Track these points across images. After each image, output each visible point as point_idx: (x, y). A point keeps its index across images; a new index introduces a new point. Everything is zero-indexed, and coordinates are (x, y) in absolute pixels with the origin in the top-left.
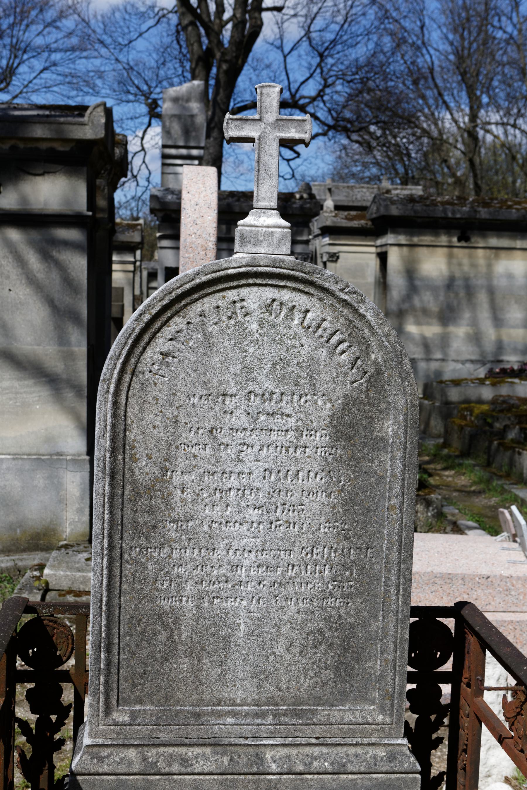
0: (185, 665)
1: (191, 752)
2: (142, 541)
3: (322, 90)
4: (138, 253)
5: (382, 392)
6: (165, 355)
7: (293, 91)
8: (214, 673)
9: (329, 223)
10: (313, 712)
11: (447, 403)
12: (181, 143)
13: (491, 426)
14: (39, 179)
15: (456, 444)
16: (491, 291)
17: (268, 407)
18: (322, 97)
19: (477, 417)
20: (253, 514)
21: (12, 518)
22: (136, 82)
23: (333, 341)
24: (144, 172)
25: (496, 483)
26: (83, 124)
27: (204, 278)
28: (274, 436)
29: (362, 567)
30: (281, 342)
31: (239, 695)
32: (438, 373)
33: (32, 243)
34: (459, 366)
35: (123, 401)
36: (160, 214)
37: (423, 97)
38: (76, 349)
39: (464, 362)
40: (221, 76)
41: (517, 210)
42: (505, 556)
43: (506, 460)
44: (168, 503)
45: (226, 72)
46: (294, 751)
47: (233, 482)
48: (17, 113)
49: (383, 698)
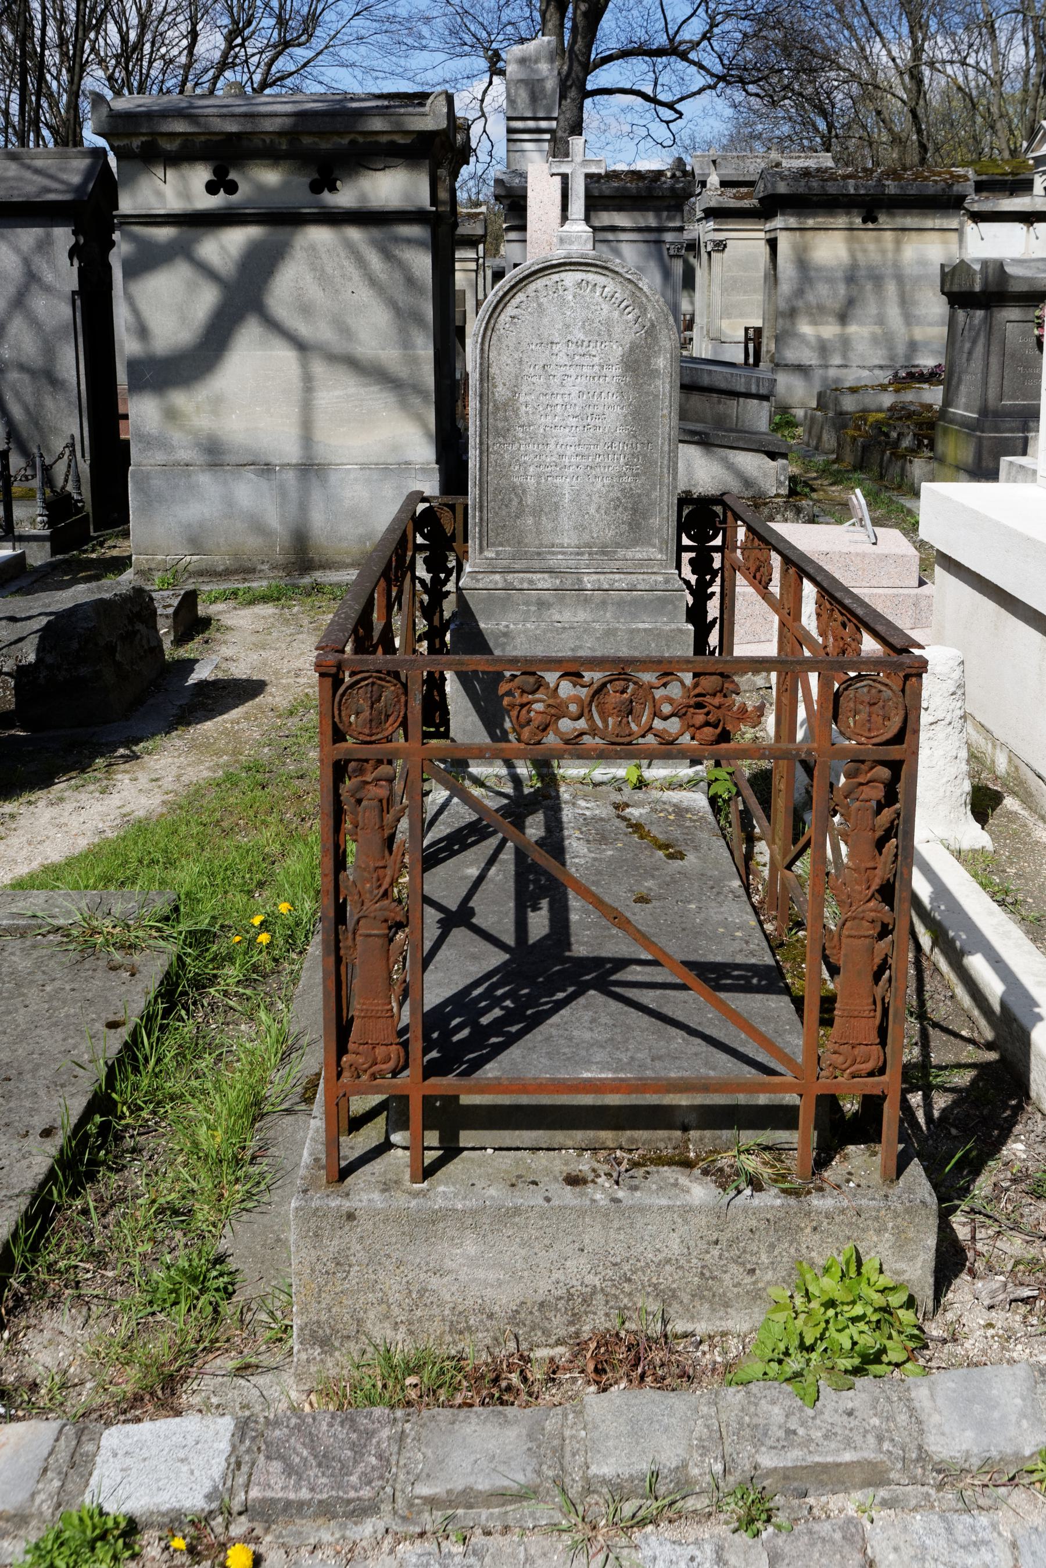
0: (530, 521)
1: (535, 577)
2: (501, 439)
3: (710, 31)
4: (481, 247)
5: (655, 339)
6: (513, 317)
7: (671, 32)
8: (549, 526)
9: (713, 204)
10: (615, 552)
11: (841, 414)
12: (529, 115)
13: (887, 435)
14: (379, 175)
15: (849, 458)
16: (900, 279)
17: (580, 350)
18: (709, 39)
19: (871, 426)
20: (573, 422)
21: (361, 530)
22: (472, 29)
23: (623, 306)
24: (485, 145)
25: (884, 495)
26: (424, 115)
27: (537, 267)
28: (585, 369)
29: (645, 456)
30: (588, 307)
31: (566, 541)
32: (837, 380)
33: (376, 244)
34: (866, 373)
35: (486, 348)
36: (507, 202)
37: (850, 27)
38: (422, 352)
39: (871, 369)
40: (579, 19)
41: (935, 181)
42: (849, 536)
43: (898, 470)
44: (517, 415)
45: (585, 14)
46: (602, 577)
47: (559, 400)
48: (355, 105)
49: (661, 543)
